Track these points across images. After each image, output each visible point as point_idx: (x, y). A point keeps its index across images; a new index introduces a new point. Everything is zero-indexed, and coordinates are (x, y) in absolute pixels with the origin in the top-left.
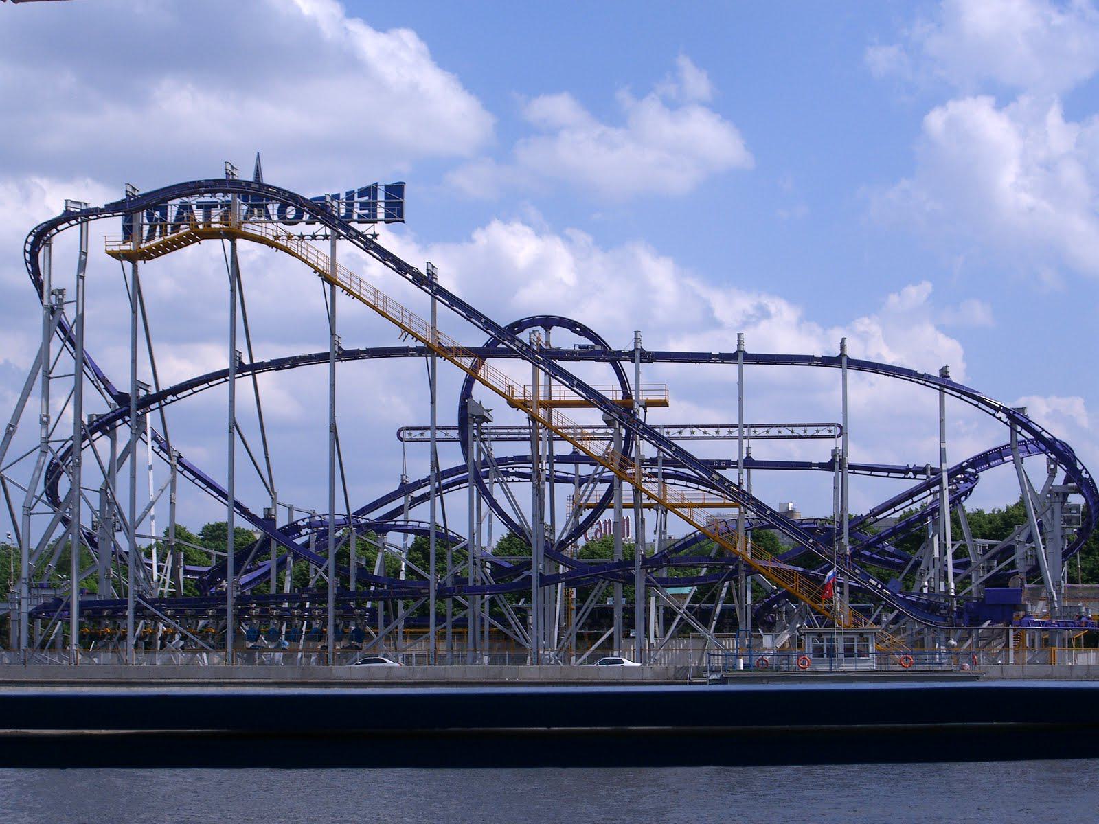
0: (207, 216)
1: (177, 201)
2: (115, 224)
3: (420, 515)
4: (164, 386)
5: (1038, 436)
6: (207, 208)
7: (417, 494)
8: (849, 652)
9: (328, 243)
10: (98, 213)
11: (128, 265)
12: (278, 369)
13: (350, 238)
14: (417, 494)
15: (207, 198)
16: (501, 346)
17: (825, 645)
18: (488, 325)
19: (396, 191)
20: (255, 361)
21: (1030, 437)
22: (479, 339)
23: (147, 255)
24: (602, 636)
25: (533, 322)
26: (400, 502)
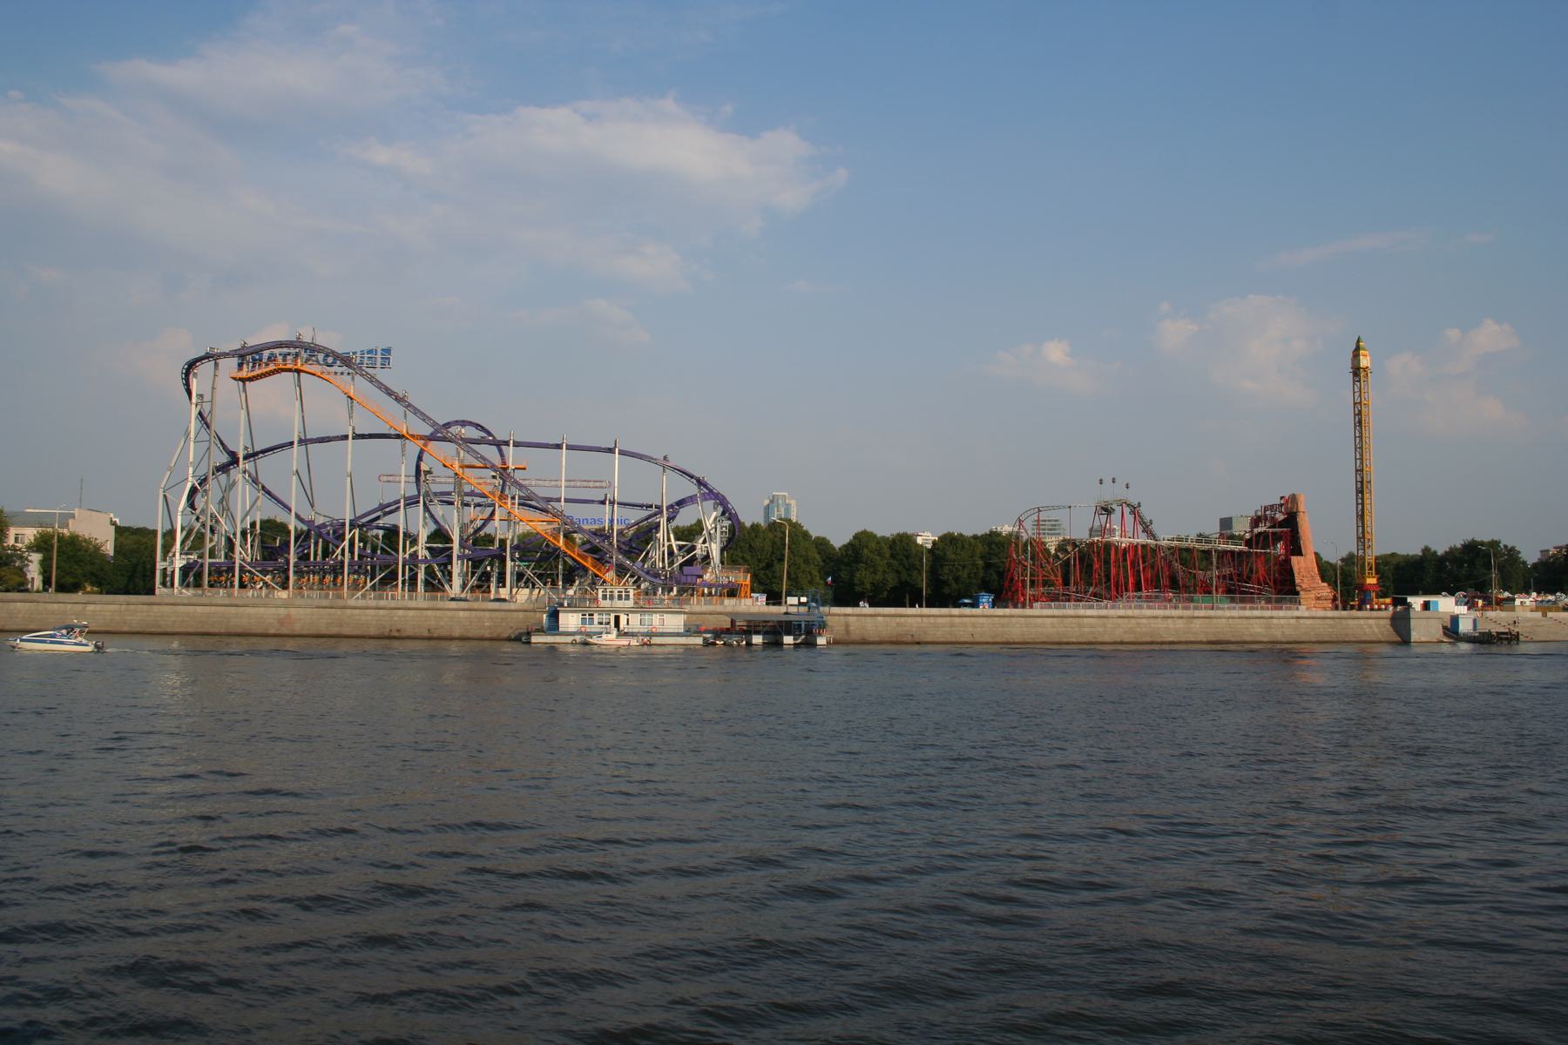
0: (284, 360)
1: (268, 351)
2: (235, 361)
3: (387, 521)
4: (257, 449)
5: (711, 491)
6: (285, 356)
7: (387, 510)
8: (620, 597)
9: (350, 377)
10: (226, 355)
11: (241, 383)
12: (329, 437)
13: (362, 375)
14: (387, 510)
15: (285, 350)
16: (439, 435)
17: (608, 594)
18: (434, 424)
19: (387, 351)
20: (308, 438)
21: (707, 491)
22: (428, 431)
23: (251, 379)
24: (398, 570)
25: (456, 423)
26: (379, 513)
